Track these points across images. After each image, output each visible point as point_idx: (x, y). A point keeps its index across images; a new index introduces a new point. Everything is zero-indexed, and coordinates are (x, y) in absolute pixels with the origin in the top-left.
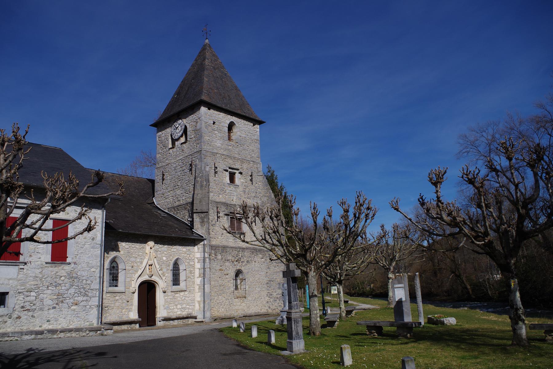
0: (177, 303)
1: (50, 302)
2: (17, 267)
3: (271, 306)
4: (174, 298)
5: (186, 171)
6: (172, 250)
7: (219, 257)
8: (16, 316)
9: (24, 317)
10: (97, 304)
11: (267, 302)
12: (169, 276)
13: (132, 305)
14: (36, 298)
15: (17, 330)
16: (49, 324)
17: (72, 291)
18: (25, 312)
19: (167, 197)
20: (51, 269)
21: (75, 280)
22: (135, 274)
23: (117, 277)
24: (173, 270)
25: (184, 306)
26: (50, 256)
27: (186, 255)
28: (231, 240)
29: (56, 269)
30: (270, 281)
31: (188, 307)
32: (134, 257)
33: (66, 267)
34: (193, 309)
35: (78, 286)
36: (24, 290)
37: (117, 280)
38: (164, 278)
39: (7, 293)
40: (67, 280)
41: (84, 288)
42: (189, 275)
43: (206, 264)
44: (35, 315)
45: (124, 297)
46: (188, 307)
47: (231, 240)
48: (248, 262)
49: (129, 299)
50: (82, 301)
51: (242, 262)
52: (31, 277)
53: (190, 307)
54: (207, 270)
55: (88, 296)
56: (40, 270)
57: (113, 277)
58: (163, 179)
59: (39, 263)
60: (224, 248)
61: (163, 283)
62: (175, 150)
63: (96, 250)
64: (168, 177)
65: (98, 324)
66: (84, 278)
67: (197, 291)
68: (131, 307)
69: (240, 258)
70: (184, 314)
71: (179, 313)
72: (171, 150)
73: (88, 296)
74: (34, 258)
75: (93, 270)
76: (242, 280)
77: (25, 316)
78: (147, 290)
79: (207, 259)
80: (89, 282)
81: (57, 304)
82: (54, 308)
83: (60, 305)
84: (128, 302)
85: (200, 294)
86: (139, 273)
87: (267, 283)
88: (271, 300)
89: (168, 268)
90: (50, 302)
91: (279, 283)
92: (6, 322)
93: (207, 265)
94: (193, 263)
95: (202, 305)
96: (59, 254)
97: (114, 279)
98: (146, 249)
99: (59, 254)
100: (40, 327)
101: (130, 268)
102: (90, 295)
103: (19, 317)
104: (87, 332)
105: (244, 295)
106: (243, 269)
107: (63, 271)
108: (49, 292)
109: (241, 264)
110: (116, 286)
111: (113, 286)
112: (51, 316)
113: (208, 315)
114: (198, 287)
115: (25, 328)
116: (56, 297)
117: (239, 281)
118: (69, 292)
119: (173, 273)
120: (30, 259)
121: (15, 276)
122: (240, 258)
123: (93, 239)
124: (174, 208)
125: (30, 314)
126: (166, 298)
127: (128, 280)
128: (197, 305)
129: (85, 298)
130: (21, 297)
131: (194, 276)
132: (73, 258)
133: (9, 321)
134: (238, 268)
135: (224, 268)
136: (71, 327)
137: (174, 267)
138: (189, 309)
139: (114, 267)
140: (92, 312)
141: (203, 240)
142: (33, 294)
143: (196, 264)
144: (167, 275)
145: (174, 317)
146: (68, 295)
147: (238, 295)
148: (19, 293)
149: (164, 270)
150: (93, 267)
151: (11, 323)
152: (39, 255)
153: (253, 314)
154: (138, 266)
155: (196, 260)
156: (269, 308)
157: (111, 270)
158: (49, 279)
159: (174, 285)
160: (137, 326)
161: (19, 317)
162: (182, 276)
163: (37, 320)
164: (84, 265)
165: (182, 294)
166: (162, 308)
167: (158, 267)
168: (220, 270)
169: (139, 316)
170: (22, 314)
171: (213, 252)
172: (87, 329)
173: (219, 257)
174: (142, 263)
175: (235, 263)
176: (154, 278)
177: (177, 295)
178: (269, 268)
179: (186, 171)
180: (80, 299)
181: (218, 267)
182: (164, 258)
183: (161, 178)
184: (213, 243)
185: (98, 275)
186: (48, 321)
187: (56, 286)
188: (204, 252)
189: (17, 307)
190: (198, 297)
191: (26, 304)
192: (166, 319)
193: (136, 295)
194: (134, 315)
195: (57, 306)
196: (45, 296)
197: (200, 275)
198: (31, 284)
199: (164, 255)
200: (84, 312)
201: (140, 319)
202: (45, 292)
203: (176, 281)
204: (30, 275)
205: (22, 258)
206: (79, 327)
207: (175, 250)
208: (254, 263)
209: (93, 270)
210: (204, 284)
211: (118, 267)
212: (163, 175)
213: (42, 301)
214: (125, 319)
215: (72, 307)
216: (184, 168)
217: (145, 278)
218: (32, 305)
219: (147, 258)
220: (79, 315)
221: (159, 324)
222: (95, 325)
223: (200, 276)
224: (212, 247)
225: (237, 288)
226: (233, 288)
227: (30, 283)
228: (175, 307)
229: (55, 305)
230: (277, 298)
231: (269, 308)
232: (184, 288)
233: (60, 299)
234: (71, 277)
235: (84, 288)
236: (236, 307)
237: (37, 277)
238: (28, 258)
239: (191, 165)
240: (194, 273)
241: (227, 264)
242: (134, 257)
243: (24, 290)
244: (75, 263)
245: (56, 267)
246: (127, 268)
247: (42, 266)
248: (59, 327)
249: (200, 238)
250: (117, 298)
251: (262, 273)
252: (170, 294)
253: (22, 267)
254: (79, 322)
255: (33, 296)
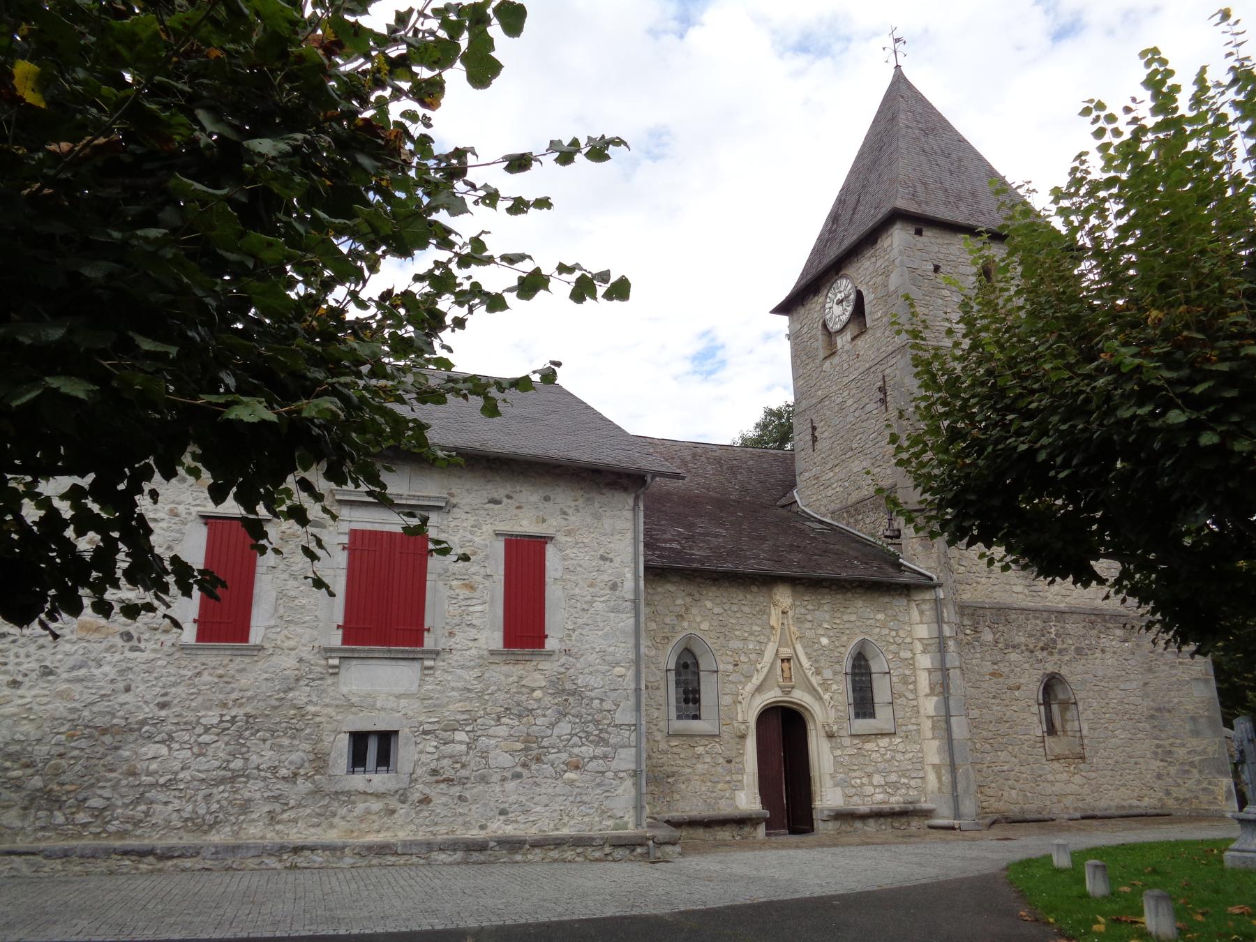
0: (870, 769)
1: (506, 760)
2: (417, 665)
3: (1173, 790)
4: (860, 753)
5: (870, 407)
6: (846, 618)
7: (988, 636)
8: (417, 796)
9: (438, 801)
10: (633, 766)
11: (1159, 777)
12: (842, 690)
13: (742, 771)
14: (469, 748)
15: (420, 836)
16: (506, 822)
17: (564, 728)
18: (442, 786)
19: (828, 483)
20: (505, 668)
21: (571, 699)
22: (745, 684)
23: (697, 691)
24: (854, 674)
25: (893, 778)
26: (501, 634)
27: (886, 631)
28: (1019, 589)
29: (517, 670)
30: (1159, 710)
31: (903, 780)
32: (737, 637)
33: (546, 665)
34: (922, 790)
35: (579, 716)
36: (436, 727)
37: (697, 701)
38: (827, 697)
39: (396, 732)
40: (549, 698)
41: (597, 723)
42: (899, 687)
43: (948, 657)
44: (467, 794)
45: (718, 748)
46: (903, 780)
47: (1019, 589)
48: (1079, 651)
49: (733, 754)
50: (591, 759)
51: (1060, 652)
52: (453, 689)
53: (913, 783)
54: (955, 674)
55: (606, 743)
56: (477, 672)
57: (686, 692)
58: (815, 439)
59: (474, 652)
60: (1001, 612)
61: (825, 708)
62: (836, 360)
63: (624, 616)
64: (824, 433)
65: (638, 825)
66: (593, 694)
67: (929, 734)
68: (739, 777)
69: (1054, 641)
70: (895, 801)
71: (877, 798)
72: (827, 364)
73: (606, 743)
74: (460, 639)
75: (619, 670)
76: (1065, 705)
77: (441, 797)
78: (784, 731)
79: (951, 643)
80: (608, 705)
81: (524, 765)
82: (518, 776)
83: (534, 767)
84: (729, 762)
85: (936, 743)
86: (756, 680)
87: (1152, 717)
88: (1172, 770)
89: (837, 667)
90: (506, 760)
91: (1193, 719)
92: (393, 812)
93: (953, 659)
94: (908, 655)
95: (946, 778)
96: (524, 625)
97: (690, 699)
98: (769, 615)
99: (524, 625)
100: (482, 827)
101: (730, 667)
102: (612, 741)
103: (426, 800)
104: (607, 850)
105: (1078, 749)
106: (1064, 671)
107: (537, 675)
108: (502, 731)
109: (1056, 657)
110: (696, 717)
111: (687, 717)
112: (511, 799)
113: (968, 807)
114: (929, 723)
115: (442, 833)
116: (520, 746)
117: (1055, 708)
118: (557, 731)
119: (854, 682)
120: (451, 642)
121: (414, 689)
122: (1054, 641)
123: (614, 587)
124: (846, 509)
125: (456, 790)
126: (838, 752)
127: (727, 700)
128: (932, 777)
129: (599, 751)
130: (431, 744)
131: (915, 691)
132: (561, 640)
133: (402, 810)
134: (1050, 668)
135: (1003, 668)
136: (565, 831)
137: (854, 667)
138: (908, 787)
139: (686, 666)
140: (620, 791)
141: (934, 587)
142: (461, 736)
143: (918, 656)
144: (835, 687)
145: (864, 809)
146: (554, 740)
147: (1058, 750)
148: (425, 733)
149: (828, 674)
150: (618, 664)
151: (407, 814)
152: (473, 633)
153: (1112, 812)
154: (753, 663)
155: (918, 647)
156: (1168, 793)
157: (678, 673)
158: (501, 696)
159: (857, 716)
160: (761, 831)
161: (426, 800)
162: (881, 691)
163: (474, 807)
164: (592, 658)
165: (884, 742)
166: (828, 782)
167: (806, 663)
168: (993, 674)
169: (762, 803)
170: (431, 792)
171: (966, 622)
172: (606, 841)
173: (988, 636)
174: (761, 653)
175: (1040, 655)
176: (800, 696)
177: (868, 746)
178: (1150, 670)
179: (870, 407)
180: (587, 750)
181: (988, 667)
182: (824, 641)
183: (809, 437)
184: (966, 597)
185: (633, 686)
186: (503, 812)
187: (520, 716)
188: (939, 620)
189: (419, 771)
190: (933, 752)
191: (446, 762)
192: (842, 816)
193: (751, 745)
194: (748, 800)
195: (525, 772)
196: (493, 742)
197: (932, 689)
198: (454, 710)
199: (821, 631)
200: (598, 791)
201: (767, 813)
202: (491, 732)
203: (864, 704)
204: (453, 684)
205: (429, 641)
206: (587, 834)
207: (853, 618)
208: (1098, 654)
209: (619, 670)
210: (948, 717)
211: (697, 664)
212: (814, 428)
213: (484, 755)
214: (724, 809)
215: (567, 776)
216: (865, 400)
217: (772, 695)
218: (458, 766)
219: (776, 638)
220: (584, 797)
221: (818, 825)
222: (631, 830)
223: (932, 693)
224: (963, 609)
225: (1051, 730)
226: (1039, 730)
227: (451, 707)
228: (865, 780)
229: (519, 769)
230: (1192, 764)
231: (1168, 793)
232: (889, 727)
233: (532, 751)
234: (566, 693)
235: (597, 723)
236: (1058, 788)
237: (469, 690)
238: (444, 640)
239: (882, 390)
240: (915, 682)
241: (1014, 656)
242: (737, 637)
243: (436, 727)
244: (567, 652)
245: (517, 662)
246: (721, 667)
247: (481, 661)
248: (532, 832)
249: (922, 581)
250: (700, 750)
251: (1128, 686)
252: (847, 741)
253: (428, 663)
254: (586, 819)
255: (461, 742)
